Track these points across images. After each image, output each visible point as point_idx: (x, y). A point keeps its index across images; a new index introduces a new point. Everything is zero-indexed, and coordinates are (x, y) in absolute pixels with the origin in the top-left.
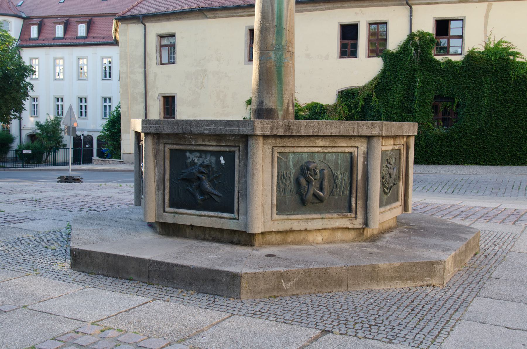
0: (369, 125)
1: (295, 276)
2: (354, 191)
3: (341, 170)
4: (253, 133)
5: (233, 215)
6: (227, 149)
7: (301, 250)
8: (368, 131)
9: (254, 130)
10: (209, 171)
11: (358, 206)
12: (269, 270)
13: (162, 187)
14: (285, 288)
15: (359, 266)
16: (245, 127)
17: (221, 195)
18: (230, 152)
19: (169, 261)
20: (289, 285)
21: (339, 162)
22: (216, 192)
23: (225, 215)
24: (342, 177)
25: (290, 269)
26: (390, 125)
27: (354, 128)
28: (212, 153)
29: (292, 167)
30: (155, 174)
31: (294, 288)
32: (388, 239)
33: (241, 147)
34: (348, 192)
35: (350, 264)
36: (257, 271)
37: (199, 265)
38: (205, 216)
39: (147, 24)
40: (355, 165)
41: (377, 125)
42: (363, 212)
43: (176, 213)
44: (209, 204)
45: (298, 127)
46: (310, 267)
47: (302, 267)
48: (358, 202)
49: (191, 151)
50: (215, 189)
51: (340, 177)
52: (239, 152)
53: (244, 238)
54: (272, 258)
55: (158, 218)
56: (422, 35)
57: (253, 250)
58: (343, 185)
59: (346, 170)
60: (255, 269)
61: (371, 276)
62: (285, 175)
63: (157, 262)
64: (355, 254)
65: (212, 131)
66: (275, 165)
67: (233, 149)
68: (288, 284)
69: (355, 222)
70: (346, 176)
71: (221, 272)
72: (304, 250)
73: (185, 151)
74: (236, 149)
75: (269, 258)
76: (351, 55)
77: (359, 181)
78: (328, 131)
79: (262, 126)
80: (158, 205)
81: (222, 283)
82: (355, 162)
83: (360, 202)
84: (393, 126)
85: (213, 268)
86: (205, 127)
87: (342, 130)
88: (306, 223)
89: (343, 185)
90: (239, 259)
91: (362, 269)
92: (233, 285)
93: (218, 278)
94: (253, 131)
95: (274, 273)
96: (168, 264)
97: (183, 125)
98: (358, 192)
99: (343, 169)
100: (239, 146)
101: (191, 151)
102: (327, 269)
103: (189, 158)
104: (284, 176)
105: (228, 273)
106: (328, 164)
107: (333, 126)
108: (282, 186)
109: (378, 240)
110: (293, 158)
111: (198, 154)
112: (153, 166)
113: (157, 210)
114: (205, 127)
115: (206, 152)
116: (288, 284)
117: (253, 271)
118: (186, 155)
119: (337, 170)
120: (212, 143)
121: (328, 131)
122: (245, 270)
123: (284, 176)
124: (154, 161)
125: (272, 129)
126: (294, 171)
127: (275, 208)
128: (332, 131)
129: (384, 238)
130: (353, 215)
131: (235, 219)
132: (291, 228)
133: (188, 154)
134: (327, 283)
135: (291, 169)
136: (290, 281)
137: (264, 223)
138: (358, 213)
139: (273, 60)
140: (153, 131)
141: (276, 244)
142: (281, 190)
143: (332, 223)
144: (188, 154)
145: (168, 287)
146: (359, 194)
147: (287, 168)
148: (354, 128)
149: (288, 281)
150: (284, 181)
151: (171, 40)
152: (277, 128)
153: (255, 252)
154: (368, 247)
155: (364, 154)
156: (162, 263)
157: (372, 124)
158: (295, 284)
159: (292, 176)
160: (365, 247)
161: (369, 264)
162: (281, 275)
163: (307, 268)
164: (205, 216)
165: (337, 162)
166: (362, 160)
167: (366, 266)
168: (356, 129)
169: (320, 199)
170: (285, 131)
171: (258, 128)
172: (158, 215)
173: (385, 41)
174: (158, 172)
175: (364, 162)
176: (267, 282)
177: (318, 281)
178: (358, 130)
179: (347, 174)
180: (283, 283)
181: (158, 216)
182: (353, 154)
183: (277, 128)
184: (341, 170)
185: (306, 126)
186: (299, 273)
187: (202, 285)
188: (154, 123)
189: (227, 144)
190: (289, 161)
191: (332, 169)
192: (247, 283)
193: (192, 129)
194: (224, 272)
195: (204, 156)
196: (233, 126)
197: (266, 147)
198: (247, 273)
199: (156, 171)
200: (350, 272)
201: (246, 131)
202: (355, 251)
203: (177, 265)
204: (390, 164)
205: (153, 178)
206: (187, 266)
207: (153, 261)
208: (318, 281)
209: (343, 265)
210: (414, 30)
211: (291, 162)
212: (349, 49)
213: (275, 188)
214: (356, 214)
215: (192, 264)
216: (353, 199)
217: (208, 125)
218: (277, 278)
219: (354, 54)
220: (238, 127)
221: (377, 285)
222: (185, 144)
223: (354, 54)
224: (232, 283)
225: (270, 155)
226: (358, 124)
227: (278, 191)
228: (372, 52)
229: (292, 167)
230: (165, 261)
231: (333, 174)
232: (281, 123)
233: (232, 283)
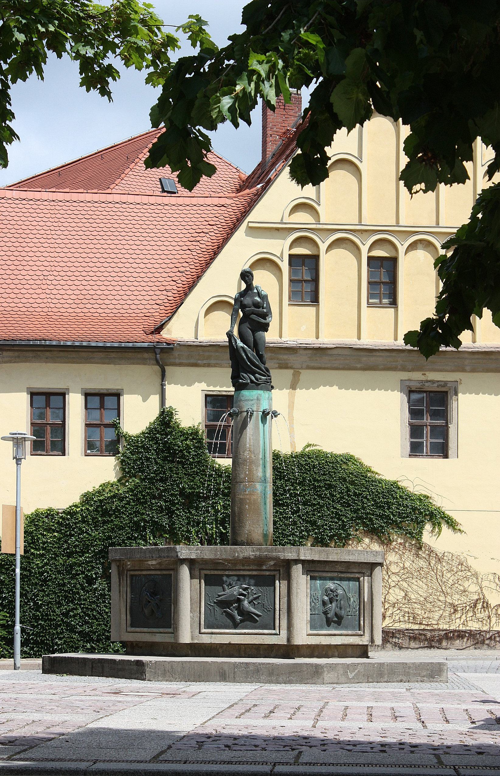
10: (248, 593)
16: (291, 553)
24: (354, 599)
34: (357, 612)
43: (212, 633)
44: (248, 620)
49: (228, 576)
51: (352, 599)
55: (192, 639)
67: (272, 573)
73: (222, 575)
101: (228, 576)
103: (226, 581)
111: (236, 578)
115: (244, 576)
118: (223, 580)
128: (350, 558)
133: (225, 578)
139: (259, 492)
144: (225, 578)
164: (245, 634)
179: (357, 595)
212: (49, 438)
219: (59, 448)
223: (59, 448)
226: (216, 555)
231: (347, 596)
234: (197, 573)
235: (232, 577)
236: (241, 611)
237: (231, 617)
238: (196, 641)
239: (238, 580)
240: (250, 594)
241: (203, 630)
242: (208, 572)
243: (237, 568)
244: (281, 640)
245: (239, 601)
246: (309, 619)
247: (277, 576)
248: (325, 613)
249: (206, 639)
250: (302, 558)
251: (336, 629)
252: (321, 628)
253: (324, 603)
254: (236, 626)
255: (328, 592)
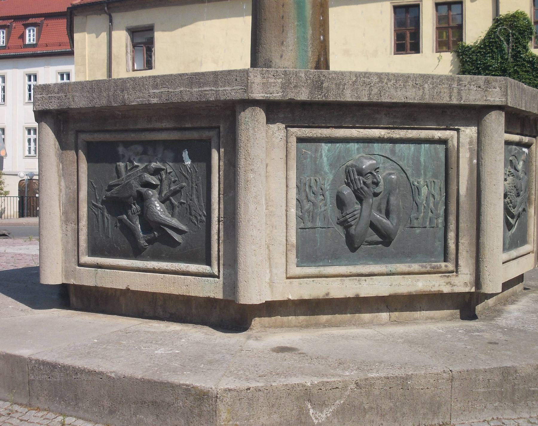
0: (481, 83)
1: (337, 393)
2: (452, 219)
3: (425, 175)
4: (245, 97)
5: (208, 268)
6: (195, 135)
7: (346, 338)
8: (479, 96)
9: (246, 89)
10: (161, 180)
11: (461, 247)
12: (279, 382)
13: (74, 216)
14: (316, 422)
15: (476, 371)
16: (229, 84)
17: (183, 227)
18: (200, 141)
19: (68, 362)
20: (324, 416)
21: (422, 159)
22: (175, 222)
23: (193, 267)
24: (428, 189)
25: (325, 380)
26: (519, 88)
27: (451, 88)
28: (167, 144)
29: (326, 168)
30: (60, 191)
31: (336, 420)
32: (516, 314)
33: (221, 129)
34: (441, 220)
35: (456, 368)
36: (253, 385)
37: (128, 372)
38: (154, 271)
39: (113, 15)
40: (454, 166)
41: (497, 85)
42: (472, 261)
44: (158, 243)
45: (338, 85)
46: (370, 375)
47: (351, 374)
48: (461, 241)
50: (173, 216)
51: (424, 191)
52: (219, 137)
53: (230, 316)
54: (287, 355)
55: (67, 276)
56: (514, 19)
57: (249, 338)
58: (431, 205)
59: (435, 176)
60: (247, 379)
61: (502, 393)
62: (313, 184)
63: (45, 363)
64: (461, 345)
65: (164, 99)
66: (293, 164)
67: (206, 134)
68: (321, 412)
69: (454, 279)
70: (437, 188)
71: (173, 386)
72: (354, 337)
74: (212, 134)
75: (280, 355)
76: (411, 50)
77: (462, 199)
78: (399, 93)
79: (265, 80)
80: (66, 252)
81: (176, 412)
82: (453, 160)
83: (466, 243)
84: (523, 89)
85: (156, 378)
86: (152, 91)
87: (426, 91)
88: (356, 282)
89: (431, 205)
90: (217, 357)
91: (481, 377)
92: (200, 416)
93: (167, 400)
94: (246, 91)
95: (290, 389)
96: (65, 369)
97: (108, 89)
98: (461, 221)
99: (429, 174)
100: (219, 127)
102: (408, 378)
104: (310, 187)
105: (188, 390)
106: (401, 163)
107: (410, 83)
108: (307, 206)
109: (500, 316)
110: (329, 150)
111: (140, 149)
112: (56, 174)
113: (66, 261)
114: (152, 91)
115: (154, 143)
116: (321, 412)
117: (244, 385)
119: (419, 176)
120: (165, 124)
121: (399, 93)
122: (224, 385)
123: (310, 187)
124: (58, 166)
125: (284, 87)
126: (331, 177)
127: (294, 252)
128: (408, 94)
129: (510, 313)
130: (451, 266)
131: (212, 276)
132: (327, 294)
133: (121, 150)
134: (406, 409)
135: (326, 173)
136: (327, 406)
137: (271, 283)
138: (460, 262)
140: (53, 106)
141: (295, 326)
142: (306, 215)
143: (409, 282)
144: (121, 150)
145: (65, 415)
146: (462, 225)
147: (317, 170)
148: (451, 88)
149: (321, 405)
150: (312, 197)
151: (147, 35)
152: (295, 87)
153: (252, 343)
154: (483, 331)
155: (471, 143)
156: (53, 366)
157: (487, 82)
158: (336, 413)
159: (327, 187)
160: (478, 331)
161: (495, 365)
162: (307, 395)
163: (362, 376)
164: (154, 271)
165: (419, 161)
166: (468, 155)
167: (491, 371)
168: (455, 91)
169: (386, 238)
170: (311, 93)
171: (255, 86)
172: (66, 271)
173: (460, 28)
174: (67, 187)
175: (471, 160)
176: (275, 409)
177: (387, 405)
178: (459, 93)
180: (311, 411)
181: (67, 273)
182: (450, 144)
183: (295, 87)
184: (425, 175)
185: (354, 83)
186: (345, 388)
187: (135, 414)
188: (56, 90)
189: (198, 125)
190: (321, 156)
191: (409, 173)
192: (229, 412)
193: (126, 96)
194: (179, 386)
195: (150, 152)
196: (205, 84)
197: (274, 127)
198: (230, 390)
199: (63, 184)
200: (456, 384)
201: (231, 92)
202: (460, 340)
203: (82, 371)
204: (516, 169)
205: (56, 198)
206: (101, 373)
207: (37, 361)
208: (387, 405)
209: (440, 370)
210: (504, 12)
211: (325, 159)
213: (293, 211)
214: (457, 265)
215: (114, 369)
216: (452, 235)
217: (156, 87)
218: (298, 399)
219: (416, 48)
220: (216, 84)
221: (514, 410)
222: (115, 131)
223: (416, 48)
224: (196, 411)
225: (283, 143)
227: (300, 218)
228: (442, 45)
229: (326, 168)
230: (61, 361)
231: (411, 185)
232: (303, 75)
233: (196, 411)
234: (71, 139)
235: (133, 147)
236: (151, 225)
237: (127, 230)
238: (72, 281)
239: (145, 153)
240: (166, 182)
241: (86, 259)
242: (88, 137)
243: (139, 126)
244: (212, 289)
245: (142, 199)
246: (293, 239)
247: (214, 143)
248: (345, 224)
249: (87, 278)
250: (258, 95)
251: (379, 258)
252: (334, 258)
253: (340, 203)
254: (137, 253)
255: (353, 175)
